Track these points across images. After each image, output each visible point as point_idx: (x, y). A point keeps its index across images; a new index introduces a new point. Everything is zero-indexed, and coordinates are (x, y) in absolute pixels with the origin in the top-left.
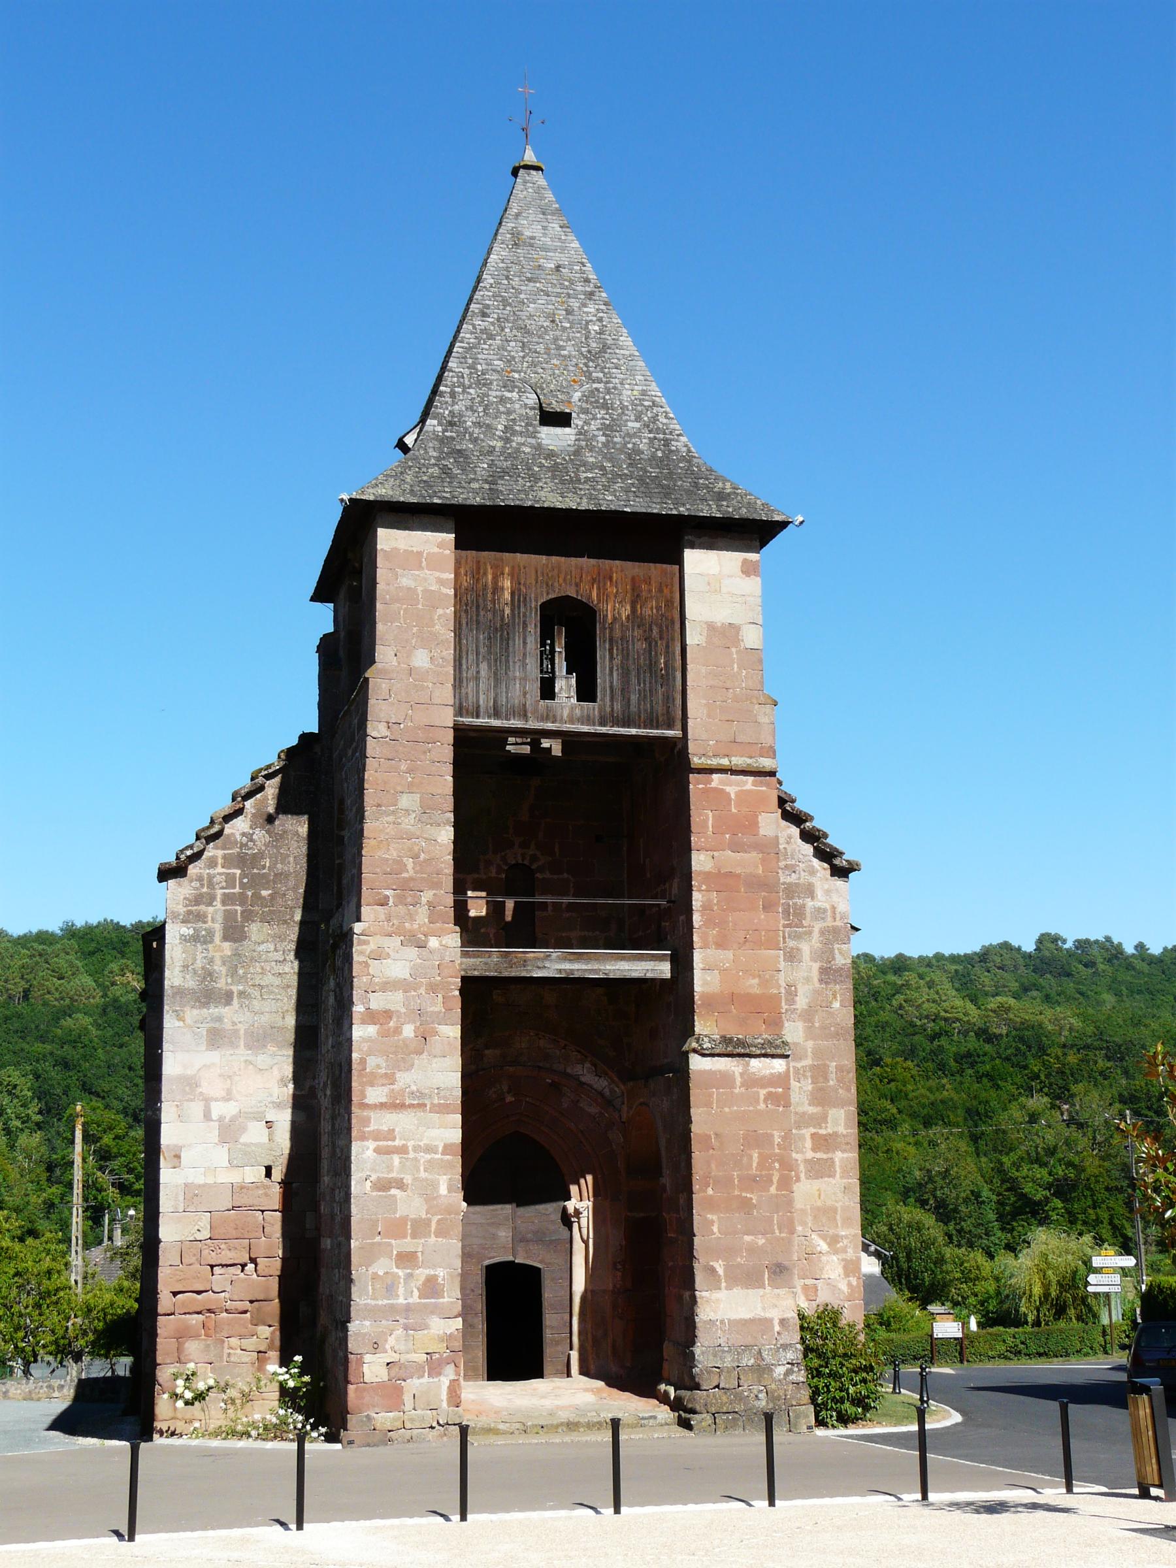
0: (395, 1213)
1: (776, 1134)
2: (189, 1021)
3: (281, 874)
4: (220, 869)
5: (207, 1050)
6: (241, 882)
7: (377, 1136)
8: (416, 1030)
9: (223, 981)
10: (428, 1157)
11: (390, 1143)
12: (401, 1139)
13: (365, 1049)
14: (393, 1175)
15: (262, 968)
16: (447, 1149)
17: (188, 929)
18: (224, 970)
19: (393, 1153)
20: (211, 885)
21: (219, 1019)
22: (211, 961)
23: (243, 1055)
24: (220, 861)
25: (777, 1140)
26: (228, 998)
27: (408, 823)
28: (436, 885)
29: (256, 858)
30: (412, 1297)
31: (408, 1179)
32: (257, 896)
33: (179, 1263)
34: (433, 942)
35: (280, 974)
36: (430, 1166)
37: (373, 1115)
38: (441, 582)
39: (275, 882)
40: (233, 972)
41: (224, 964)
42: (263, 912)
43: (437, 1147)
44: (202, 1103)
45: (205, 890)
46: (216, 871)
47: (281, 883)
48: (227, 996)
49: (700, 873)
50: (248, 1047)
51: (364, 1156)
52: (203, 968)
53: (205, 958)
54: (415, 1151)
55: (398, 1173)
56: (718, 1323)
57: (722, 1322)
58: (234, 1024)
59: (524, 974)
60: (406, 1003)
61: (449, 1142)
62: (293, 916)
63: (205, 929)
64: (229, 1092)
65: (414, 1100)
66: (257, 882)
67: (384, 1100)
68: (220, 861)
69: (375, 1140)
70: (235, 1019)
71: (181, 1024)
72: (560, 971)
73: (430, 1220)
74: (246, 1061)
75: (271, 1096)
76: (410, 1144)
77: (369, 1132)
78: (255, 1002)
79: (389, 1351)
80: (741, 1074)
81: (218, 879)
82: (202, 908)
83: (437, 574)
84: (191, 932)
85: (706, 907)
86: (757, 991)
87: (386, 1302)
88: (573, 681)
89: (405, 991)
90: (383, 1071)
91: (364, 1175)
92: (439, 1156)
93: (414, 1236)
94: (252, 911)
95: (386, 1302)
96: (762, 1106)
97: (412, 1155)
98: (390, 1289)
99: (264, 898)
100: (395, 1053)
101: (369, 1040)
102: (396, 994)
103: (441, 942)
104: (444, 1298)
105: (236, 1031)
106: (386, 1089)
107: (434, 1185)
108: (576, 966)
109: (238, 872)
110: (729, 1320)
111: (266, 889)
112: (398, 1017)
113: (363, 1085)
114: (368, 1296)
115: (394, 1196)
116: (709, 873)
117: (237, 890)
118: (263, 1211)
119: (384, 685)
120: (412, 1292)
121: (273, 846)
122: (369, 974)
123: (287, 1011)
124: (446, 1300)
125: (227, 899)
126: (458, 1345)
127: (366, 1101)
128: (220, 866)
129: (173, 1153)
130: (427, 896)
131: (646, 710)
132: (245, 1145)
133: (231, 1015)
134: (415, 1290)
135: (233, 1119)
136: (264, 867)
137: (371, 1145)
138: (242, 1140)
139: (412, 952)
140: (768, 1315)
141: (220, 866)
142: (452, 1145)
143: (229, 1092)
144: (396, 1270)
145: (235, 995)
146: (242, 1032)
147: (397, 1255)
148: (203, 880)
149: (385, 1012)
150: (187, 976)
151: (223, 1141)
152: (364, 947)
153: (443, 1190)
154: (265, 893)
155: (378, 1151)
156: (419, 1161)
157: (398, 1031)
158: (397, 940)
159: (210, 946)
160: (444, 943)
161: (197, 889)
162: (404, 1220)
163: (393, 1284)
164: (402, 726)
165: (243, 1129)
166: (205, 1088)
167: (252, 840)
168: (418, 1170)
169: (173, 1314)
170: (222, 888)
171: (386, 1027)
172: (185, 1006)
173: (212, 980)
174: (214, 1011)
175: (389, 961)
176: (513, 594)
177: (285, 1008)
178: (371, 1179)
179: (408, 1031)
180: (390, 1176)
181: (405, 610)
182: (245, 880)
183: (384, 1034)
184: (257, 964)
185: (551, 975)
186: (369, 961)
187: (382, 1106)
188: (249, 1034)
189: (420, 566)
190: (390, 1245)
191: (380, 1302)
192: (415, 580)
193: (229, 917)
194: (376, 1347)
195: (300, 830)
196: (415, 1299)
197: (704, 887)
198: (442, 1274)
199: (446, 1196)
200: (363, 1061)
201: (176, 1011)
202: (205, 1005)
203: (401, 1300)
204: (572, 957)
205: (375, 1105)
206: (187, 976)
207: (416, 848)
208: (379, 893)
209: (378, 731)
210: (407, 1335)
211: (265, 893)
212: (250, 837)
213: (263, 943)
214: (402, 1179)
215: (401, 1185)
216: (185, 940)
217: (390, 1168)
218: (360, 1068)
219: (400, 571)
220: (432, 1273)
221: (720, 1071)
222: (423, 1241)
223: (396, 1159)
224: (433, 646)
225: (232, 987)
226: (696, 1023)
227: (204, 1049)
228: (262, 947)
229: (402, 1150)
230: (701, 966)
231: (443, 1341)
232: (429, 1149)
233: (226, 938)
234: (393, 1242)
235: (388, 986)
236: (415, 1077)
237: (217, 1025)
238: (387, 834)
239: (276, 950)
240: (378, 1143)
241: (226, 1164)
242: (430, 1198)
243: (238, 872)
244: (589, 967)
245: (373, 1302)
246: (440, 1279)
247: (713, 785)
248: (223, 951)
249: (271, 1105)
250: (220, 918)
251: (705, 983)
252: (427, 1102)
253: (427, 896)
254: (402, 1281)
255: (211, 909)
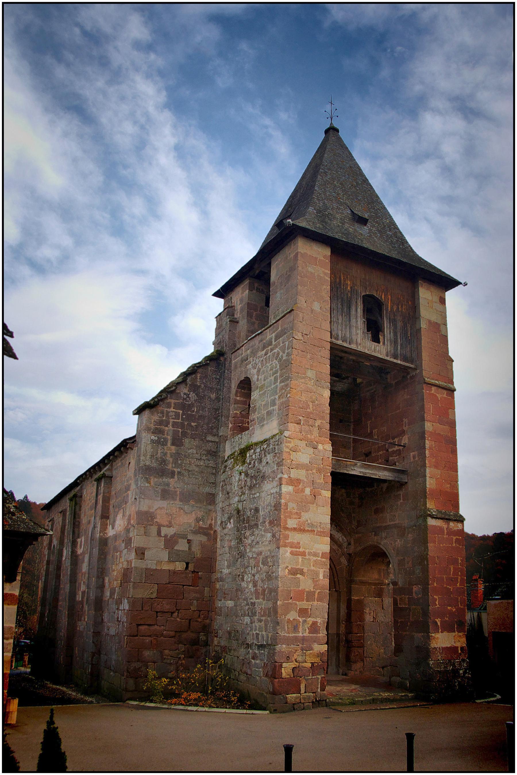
0: (299, 587)
1: (459, 558)
2: (152, 484)
3: (201, 416)
4: (172, 409)
5: (160, 500)
6: (182, 417)
7: (292, 545)
8: (311, 490)
9: (170, 465)
10: (315, 558)
11: (298, 550)
12: (302, 548)
13: (288, 498)
14: (299, 567)
15: (190, 461)
16: (323, 555)
17: (155, 437)
18: (171, 460)
19: (299, 555)
20: (167, 416)
21: (168, 485)
22: (165, 454)
23: (178, 504)
24: (173, 405)
25: (460, 561)
26: (172, 474)
27: (311, 384)
28: (322, 418)
29: (190, 406)
30: (305, 633)
31: (305, 570)
32: (189, 425)
33: (141, 609)
34: (320, 447)
35: (198, 465)
36: (316, 563)
37: (291, 534)
38: (325, 274)
39: (198, 419)
40: (175, 462)
41: (171, 456)
42: (192, 433)
43: (319, 553)
44: (157, 527)
45: (164, 418)
46: (170, 410)
47: (201, 421)
48: (172, 474)
49: (428, 431)
50: (181, 500)
51: (285, 555)
52: (161, 458)
53: (162, 452)
54: (309, 555)
55: (301, 566)
56: (438, 649)
57: (439, 648)
58: (175, 488)
59: (345, 472)
60: (307, 476)
61: (324, 551)
62: (206, 438)
63: (163, 438)
64: (170, 522)
65: (309, 528)
66: (190, 418)
67: (295, 526)
68: (173, 405)
69: (291, 547)
70: (175, 486)
71: (149, 485)
72: (361, 472)
73: (315, 592)
74: (179, 508)
75: (191, 527)
76: (307, 551)
77: (288, 543)
78: (185, 478)
79: (294, 661)
80: (447, 529)
81: (171, 414)
82: (163, 427)
83: (323, 270)
84: (156, 438)
85: (431, 448)
86: (449, 490)
87: (293, 635)
88: (370, 335)
89: (307, 470)
90: (296, 511)
91: (285, 566)
92: (319, 559)
93: (307, 601)
94: (187, 432)
95: (293, 635)
96: (454, 545)
97: (307, 557)
98: (296, 628)
99: (192, 426)
100: (301, 502)
101: (289, 493)
102: (303, 471)
103: (324, 447)
104: (320, 634)
105: (176, 492)
106: (296, 521)
107: (317, 574)
108: (367, 471)
109: (181, 412)
110: (442, 647)
111: (194, 422)
112: (304, 483)
113: (286, 517)
114: (285, 631)
115: (299, 578)
116: (431, 432)
117: (180, 420)
118: (158, 584)
119: (301, 315)
120: (306, 630)
121: (198, 402)
122: (290, 459)
123: (201, 484)
124: (321, 635)
125: (175, 424)
126: (325, 658)
127: (287, 526)
128: (172, 408)
129: (141, 552)
130: (318, 423)
131: (403, 354)
132: (177, 550)
133: (173, 483)
134: (307, 629)
135: (172, 536)
136: (193, 411)
137: (289, 550)
138: (175, 548)
139: (311, 450)
140: (456, 645)
141: (172, 408)
142: (326, 553)
143: (170, 522)
144: (298, 618)
145: (176, 473)
146: (178, 493)
147: (299, 610)
148: (164, 413)
149: (297, 480)
150: (153, 461)
151: (166, 547)
152: (289, 444)
153: (321, 577)
154: (193, 424)
155: (292, 553)
156: (311, 560)
157: (303, 491)
158: (304, 443)
159: (165, 447)
160: (325, 447)
161: (160, 417)
162: (303, 591)
163: (297, 625)
164: (308, 336)
165: (176, 542)
166: (158, 519)
167: (188, 397)
168: (310, 566)
169: (137, 636)
170: (173, 419)
171: (297, 488)
172: (151, 476)
173: (165, 464)
174: (165, 480)
175: (300, 453)
176: (351, 288)
177: (200, 483)
178: (288, 568)
179: (308, 491)
180: (297, 567)
181: (310, 282)
182: (184, 417)
183: (296, 492)
184: (188, 459)
185: (357, 474)
186: (291, 452)
187: (295, 529)
188: (182, 494)
189: (316, 264)
190: (296, 604)
191: (291, 635)
192: (314, 270)
193: (175, 433)
194: (288, 659)
195: (212, 396)
196: (306, 634)
197: (430, 439)
198: (319, 621)
199: (322, 580)
200: (286, 505)
201: (147, 478)
202: (162, 476)
203: (300, 634)
204: (366, 466)
205: (291, 528)
206: (153, 461)
207: (314, 397)
208: (297, 418)
209: (298, 336)
210: (303, 653)
211: (193, 424)
212: (187, 396)
213: (191, 449)
214: (303, 569)
215: (302, 573)
216: (153, 442)
217: (297, 562)
218: (285, 508)
219: (308, 264)
220: (315, 620)
221: (439, 526)
222: (311, 603)
223: (300, 558)
224: (322, 302)
225: (175, 469)
226: (427, 503)
227: (159, 499)
228: (190, 451)
229: (303, 554)
230: (429, 475)
231: (319, 656)
232: (315, 555)
233: (173, 444)
234: (298, 603)
235: (299, 466)
236: (310, 516)
237: (166, 488)
238: (301, 388)
239: (197, 453)
240: (292, 549)
241: (167, 559)
242: (315, 581)
243: (181, 412)
244: (373, 472)
245: (287, 635)
246: (318, 624)
247: (432, 392)
248: (171, 450)
249: (190, 531)
250: (171, 433)
251: (430, 484)
252: (315, 530)
253: (318, 423)
254: (301, 624)
255: (167, 428)
